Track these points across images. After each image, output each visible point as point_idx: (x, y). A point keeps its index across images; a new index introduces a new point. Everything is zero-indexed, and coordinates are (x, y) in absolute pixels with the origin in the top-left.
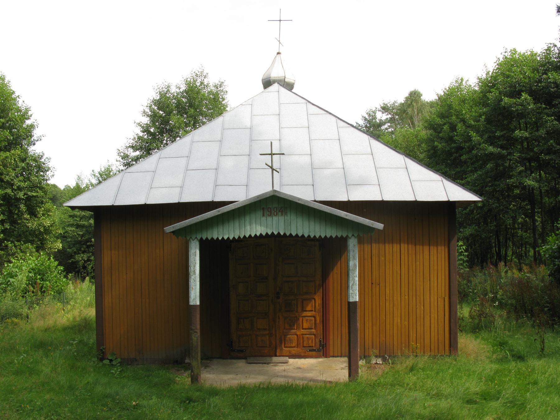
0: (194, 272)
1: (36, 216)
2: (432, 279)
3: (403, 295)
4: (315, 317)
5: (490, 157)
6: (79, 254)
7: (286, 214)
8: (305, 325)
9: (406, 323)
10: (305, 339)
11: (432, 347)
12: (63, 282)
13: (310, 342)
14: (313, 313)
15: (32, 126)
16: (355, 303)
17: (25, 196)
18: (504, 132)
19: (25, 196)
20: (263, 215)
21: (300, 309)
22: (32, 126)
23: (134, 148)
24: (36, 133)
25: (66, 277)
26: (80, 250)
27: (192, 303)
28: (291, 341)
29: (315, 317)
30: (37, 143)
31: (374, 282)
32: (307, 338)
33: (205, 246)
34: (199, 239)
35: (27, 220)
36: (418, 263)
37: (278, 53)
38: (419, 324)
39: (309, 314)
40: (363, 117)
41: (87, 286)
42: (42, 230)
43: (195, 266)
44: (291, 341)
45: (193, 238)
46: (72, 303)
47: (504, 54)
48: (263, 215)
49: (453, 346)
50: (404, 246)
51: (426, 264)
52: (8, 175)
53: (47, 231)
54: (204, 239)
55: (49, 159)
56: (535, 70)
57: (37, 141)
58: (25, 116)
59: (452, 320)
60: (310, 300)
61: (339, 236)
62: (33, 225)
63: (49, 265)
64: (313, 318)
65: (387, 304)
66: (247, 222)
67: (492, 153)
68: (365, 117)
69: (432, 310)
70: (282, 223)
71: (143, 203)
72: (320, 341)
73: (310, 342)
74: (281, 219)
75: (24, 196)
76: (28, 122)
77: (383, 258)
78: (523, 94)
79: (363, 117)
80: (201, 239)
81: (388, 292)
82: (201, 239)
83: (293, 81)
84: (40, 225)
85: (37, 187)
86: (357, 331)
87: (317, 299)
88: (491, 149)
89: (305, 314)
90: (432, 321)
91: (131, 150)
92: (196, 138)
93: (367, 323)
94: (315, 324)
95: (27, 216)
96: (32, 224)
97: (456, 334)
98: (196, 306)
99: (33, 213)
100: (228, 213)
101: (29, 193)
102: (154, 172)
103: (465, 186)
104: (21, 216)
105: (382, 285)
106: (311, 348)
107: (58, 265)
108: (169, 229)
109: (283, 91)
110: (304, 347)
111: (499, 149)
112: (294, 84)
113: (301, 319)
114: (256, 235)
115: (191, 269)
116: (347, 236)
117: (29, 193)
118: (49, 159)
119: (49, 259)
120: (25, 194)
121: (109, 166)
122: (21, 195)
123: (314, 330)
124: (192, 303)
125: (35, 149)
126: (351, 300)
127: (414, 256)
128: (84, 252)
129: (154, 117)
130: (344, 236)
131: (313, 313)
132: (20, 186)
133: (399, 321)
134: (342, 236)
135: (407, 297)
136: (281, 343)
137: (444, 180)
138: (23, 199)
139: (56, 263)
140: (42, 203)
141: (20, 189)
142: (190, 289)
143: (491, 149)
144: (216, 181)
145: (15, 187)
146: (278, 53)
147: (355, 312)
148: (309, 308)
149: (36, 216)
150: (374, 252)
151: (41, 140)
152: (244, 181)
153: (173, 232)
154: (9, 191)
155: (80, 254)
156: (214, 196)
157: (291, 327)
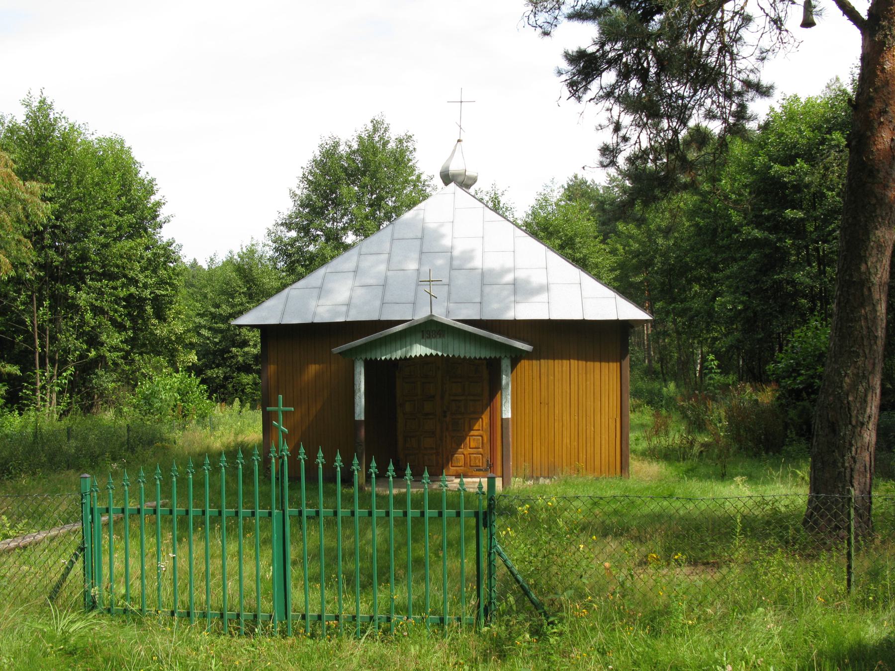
0: (360, 390)
1: (165, 320)
2: (603, 399)
3: (572, 415)
4: (482, 436)
5: (756, 243)
6: (212, 368)
7: (444, 336)
8: (472, 445)
9: (576, 444)
10: (472, 458)
11: (603, 469)
12: (207, 404)
13: (477, 461)
14: (480, 432)
15: (158, 204)
16: (507, 419)
17: (152, 295)
18: (775, 210)
19: (152, 295)
20: (423, 338)
21: (467, 429)
22: (158, 204)
23: (288, 226)
24: (163, 213)
25: (209, 398)
26: (214, 362)
27: (357, 418)
28: (458, 460)
29: (482, 436)
30: (164, 226)
31: (542, 401)
32: (475, 457)
33: (372, 368)
34: (364, 358)
35: (155, 325)
36: (588, 383)
37: (459, 141)
38: (588, 445)
41: (213, 416)
42: (173, 338)
43: (360, 384)
44: (458, 460)
45: (359, 358)
46: (221, 428)
47: (782, 101)
48: (423, 338)
49: (624, 467)
50: (574, 362)
51: (598, 383)
52: (131, 269)
53: (180, 339)
54: (866, 18)
55: (181, 246)
56: (816, 128)
57: (164, 223)
58: (149, 190)
59: (623, 442)
60: (477, 419)
61: (493, 357)
62: (162, 332)
63: (190, 383)
64: (480, 438)
65: (556, 424)
66: (408, 343)
67: (756, 239)
69: (603, 431)
70: (440, 345)
71: (310, 322)
72: (488, 461)
73: (477, 461)
75: (150, 295)
76: (154, 199)
77: (552, 378)
78: (799, 160)
80: (366, 359)
81: (557, 412)
82: (366, 359)
83: (476, 175)
84: (171, 332)
85: (167, 283)
86: (509, 445)
87: (484, 419)
88: (757, 233)
90: (603, 442)
93: (535, 443)
94: (482, 443)
95: (154, 321)
96: (161, 331)
97: (628, 457)
98: (361, 421)
99: (160, 316)
100: (386, 337)
101: (156, 291)
102: (321, 288)
103: (640, 305)
104: (148, 320)
105: (551, 404)
106: (478, 468)
107: (200, 383)
108: (336, 350)
109: (459, 190)
110: (471, 466)
111: (766, 233)
112: (476, 177)
113: (468, 438)
114: (416, 356)
115: (357, 387)
116: (500, 357)
117: (156, 291)
118: (181, 246)
119: (190, 376)
120: (151, 293)
121: (253, 245)
122: (147, 293)
123: (481, 450)
124: (357, 418)
125: (165, 234)
126: (504, 417)
127: (584, 375)
129: (314, 185)
130: (498, 357)
131: (480, 432)
132: (146, 282)
133: (568, 441)
134: (495, 357)
135: (576, 418)
136: (448, 463)
137: (618, 297)
138: (150, 299)
140: (171, 303)
141: (145, 286)
142: (356, 405)
143: (757, 233)
144: (383, 299)
146: (459, 141)
147: (507, 428)
148: (476, 427)
149: (165, 320)
150: (542, 371)
151: (169, 221)
152: (412, 299)
153: (340, 353)
154: (133, 290)
155: (213, 368)
156: (381, 314)
157: (459, 446)
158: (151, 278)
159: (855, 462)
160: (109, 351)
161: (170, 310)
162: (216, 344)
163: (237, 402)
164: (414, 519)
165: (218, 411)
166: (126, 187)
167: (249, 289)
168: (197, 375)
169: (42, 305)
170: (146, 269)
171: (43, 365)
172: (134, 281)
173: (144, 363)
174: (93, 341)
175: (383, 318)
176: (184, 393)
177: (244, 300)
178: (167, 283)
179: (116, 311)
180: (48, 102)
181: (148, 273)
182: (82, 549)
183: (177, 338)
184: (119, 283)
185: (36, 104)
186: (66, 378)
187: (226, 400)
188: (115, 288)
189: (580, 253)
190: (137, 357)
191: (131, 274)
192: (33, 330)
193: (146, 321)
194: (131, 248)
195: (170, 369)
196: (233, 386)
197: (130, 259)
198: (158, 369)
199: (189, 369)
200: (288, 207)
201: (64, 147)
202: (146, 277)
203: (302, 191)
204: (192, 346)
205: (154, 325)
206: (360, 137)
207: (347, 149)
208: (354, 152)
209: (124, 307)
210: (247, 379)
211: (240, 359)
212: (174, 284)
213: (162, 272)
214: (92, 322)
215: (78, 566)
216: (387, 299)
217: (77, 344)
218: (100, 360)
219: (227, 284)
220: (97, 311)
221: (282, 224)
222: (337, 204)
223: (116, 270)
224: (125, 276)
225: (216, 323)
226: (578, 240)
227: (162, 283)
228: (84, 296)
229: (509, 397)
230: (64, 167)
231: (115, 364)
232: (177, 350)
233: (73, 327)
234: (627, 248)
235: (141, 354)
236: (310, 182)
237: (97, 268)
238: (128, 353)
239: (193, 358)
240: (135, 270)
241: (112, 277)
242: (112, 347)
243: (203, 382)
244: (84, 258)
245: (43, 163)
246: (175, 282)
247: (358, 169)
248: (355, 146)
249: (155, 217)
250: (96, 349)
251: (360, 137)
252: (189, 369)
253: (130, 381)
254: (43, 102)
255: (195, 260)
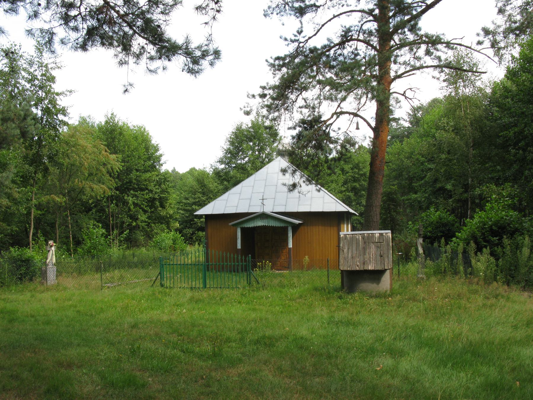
6: (185, 229)
8: (283, 258)
25: (185, 243)
33: (243, 230)
39: (284, 254)
40: (407, 113)
42: (168, 216)
50: (320, 227)
53: (171, 217)
58: (156, 149)
68: (409, 113)
70: (266, 222)
74: (266, 220)
76: (158, 154)
79: (407, 113)
85: (165, 191)
89: (283, 254)
91: (218, 164)
92: (244, 185)
96: (163, 213)
99: (163, 207)
115: (238, 237)
119: (177, 233)
120: (158, 196)
121: (204, 168)
122: (156, 196)
128: (189, 228)
129: (232, 143)
139: (180, 235)
141: (156, 193)
145: (154, 192)
148: (284, 252)
158: (158, 189)
159: (77, 225)
160: (141, 223)
161: (166, 203)
162: (187, 217)
163: (197, 245)
164: (226, 265)
165: (189, 248)
166: (147, 149)
167: (202, 190)
168: (180, 233)
169: (113, 203)
170: (156, 185)
171: (113, 230)
172: (151, 191)
173: (156, 228)
174: (134, 218)
175: (250, 211)
176: (174, 241)
177: (200, 196)
178: (165, 191)
179: (143, 204)
180: (115, 114)
181: (157, 187)
182: (160, 273)
183: (170, 216)
184: (145, 192)
185: (110, 116)
186: (126, 234)
187: (192, 244)
188: (143, 195)
189: (363, 171)
190: (153, 225)
191: (150, 188)
192: (109, 213)
193: (156, 208)
194: (150, 177)
195: (168, 230)
196: (196, 238)
197: (149, 181)
198: (163, 230)
199: (176, 230)
200: (220, 154)
201: (121, 134)
202: (156, 189)
203: (227, 146)
204: (176, 219)
205: (160, 210)
206: (252, 121)
207: (247, 127)
208: (250, 128)
209: (147, 202)
210: (201, 234)
211: (199, 224)
212: (169, 192)
213: (163, 186)
214: (134, 210)
215: (159, 277)
216: (277, 191)
217: (128, 220)
218: (137, 227)
219: (192, 188)
220: (135, 205)
221: (218, 162)
222: (243, 151)
223: (144, 187)
224: (147, 189)
225: (187, 207)
226: (361, 165)
227: (163, 191)
228: (131, 199)
229: (291, 240)
230: (122, 144)
231: (143, 228)
232: (170, 221)
233: (126, 212)
234: (389, 167)
235: (154, 223)
236: (229, 141)
237: (136, 186)
238: (149, 223)
239: (177, 225)
240: (151, 186)
241: (142, 190)
242: (143, 220)
243: (182, 236)
244: (130, 182)
245: (113, 141)
246: (169, 191)
247: (252, 135)
248: (250, 125)
249: (159, 161)
250: (136, 221)
251: (252, 121)
252: (176, 230)
253: (149, 236)
254: (112, 114)
255: (174, 168)
